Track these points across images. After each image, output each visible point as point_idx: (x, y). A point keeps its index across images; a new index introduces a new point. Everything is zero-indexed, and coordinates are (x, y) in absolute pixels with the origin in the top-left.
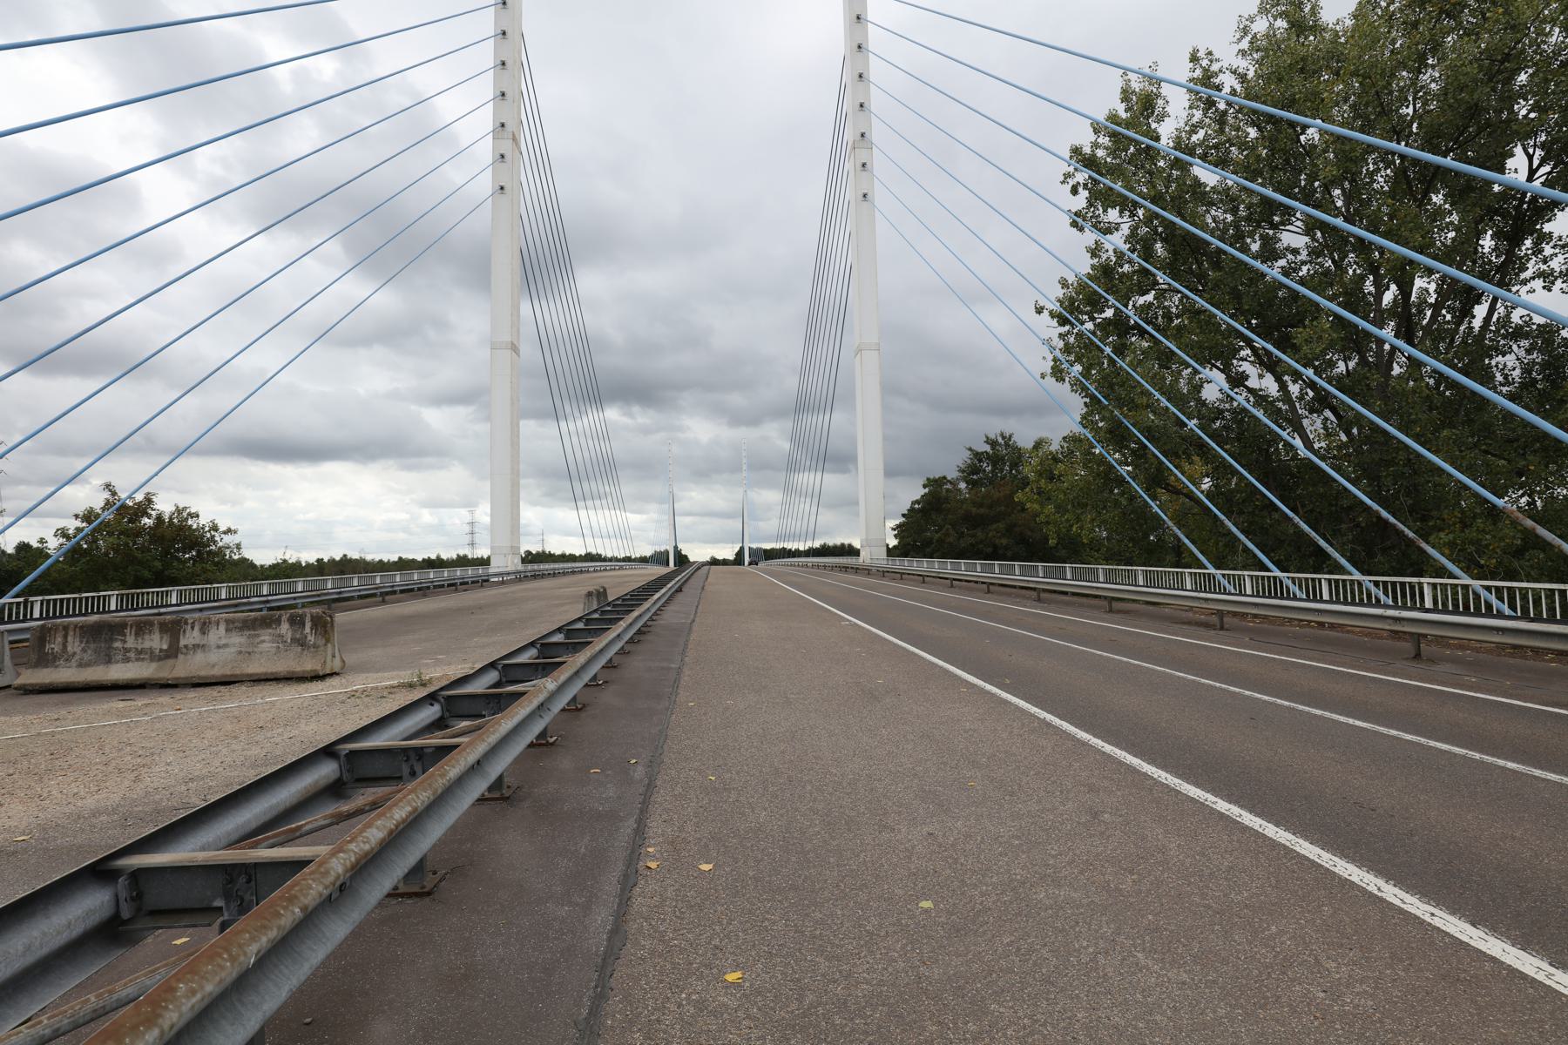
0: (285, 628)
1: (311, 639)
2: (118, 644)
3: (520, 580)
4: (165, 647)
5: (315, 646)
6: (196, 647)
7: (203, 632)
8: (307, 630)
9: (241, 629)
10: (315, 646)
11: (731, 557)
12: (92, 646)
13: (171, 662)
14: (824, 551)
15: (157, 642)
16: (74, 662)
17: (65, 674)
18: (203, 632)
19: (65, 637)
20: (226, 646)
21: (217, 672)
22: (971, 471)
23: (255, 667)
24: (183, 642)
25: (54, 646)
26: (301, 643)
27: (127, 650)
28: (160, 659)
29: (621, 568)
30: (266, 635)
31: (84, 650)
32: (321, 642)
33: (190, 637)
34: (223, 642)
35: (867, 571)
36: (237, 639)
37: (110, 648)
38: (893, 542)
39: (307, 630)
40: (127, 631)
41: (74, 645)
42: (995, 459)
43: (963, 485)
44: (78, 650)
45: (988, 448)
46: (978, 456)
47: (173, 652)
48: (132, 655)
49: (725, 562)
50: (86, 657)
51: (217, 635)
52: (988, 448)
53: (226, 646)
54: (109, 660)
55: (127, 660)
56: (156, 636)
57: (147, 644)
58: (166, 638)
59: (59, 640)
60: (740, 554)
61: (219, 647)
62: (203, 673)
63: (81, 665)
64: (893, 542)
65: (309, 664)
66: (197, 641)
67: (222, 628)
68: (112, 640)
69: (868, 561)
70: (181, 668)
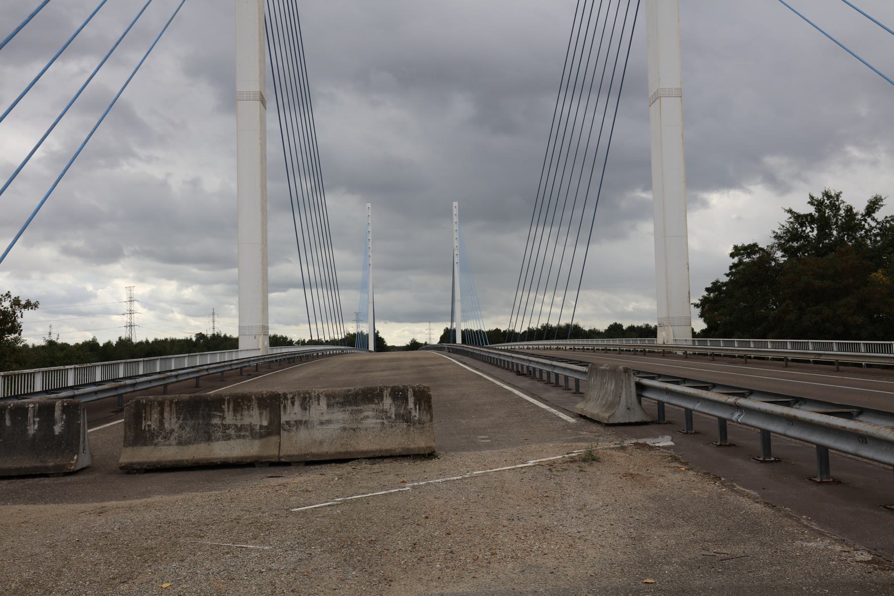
0: (387, 402)
1: (415, 414)
2: (216, 421)
3: (686, 356)
4: (265, 423)
5: (420, 422)
6: (299, 423)
7: (304, 407)
8: (411, 405)
9: (343, 404)
10: (420, 422)
11: (435, 340)
12: (190, 422)
13: (274, 439)
14: (547, 333)
15: (256, 418)
16: (173, 440)
17: (168, 452)
18: (304, 407)
19: (162, 413)
20: (329, 422)
21: (328, 449)
22: (790, 238)
23: (366, 443)
24: (284, 419)
25: (151, 422)
26: (406, 418)
27: (226, 427)
28: (261, 436)
29: (342, 353)
30: (369, 410)
31: (182, 427)
32: (426, 418)
33: (292, 413)
34: (326, 417)
35: (666, 353)
36: (340, 416)
37: (208, 424)
38: (700, 325)
39: (411, 405)
40: (225, 407)
41: (171, 422)
42: (822, 223)
43: (779, 254)
44: (176, 427)
45: (811, 210)
46: (801, 219)
47: (274, 429)
48: (232, 432)
49: (426, 347)
50: (185, 434)
51: (319, 410)
52: (811, 210)
53: (329, 422)
54: (209, 439)
55: (228, 438)
56: (255, 412)
57: (247, 421)
58: (266, 414)
59: (155, 416)
60: (448, 336)
61: (322, 423)
62: (314, 450)
63: (180, 443)
64: (700, 325)
65: (420, 442)
66: (299, 417)
67: (323, 402)
68: (210, 416)
69: (671, 342)
70: (295, 443)
